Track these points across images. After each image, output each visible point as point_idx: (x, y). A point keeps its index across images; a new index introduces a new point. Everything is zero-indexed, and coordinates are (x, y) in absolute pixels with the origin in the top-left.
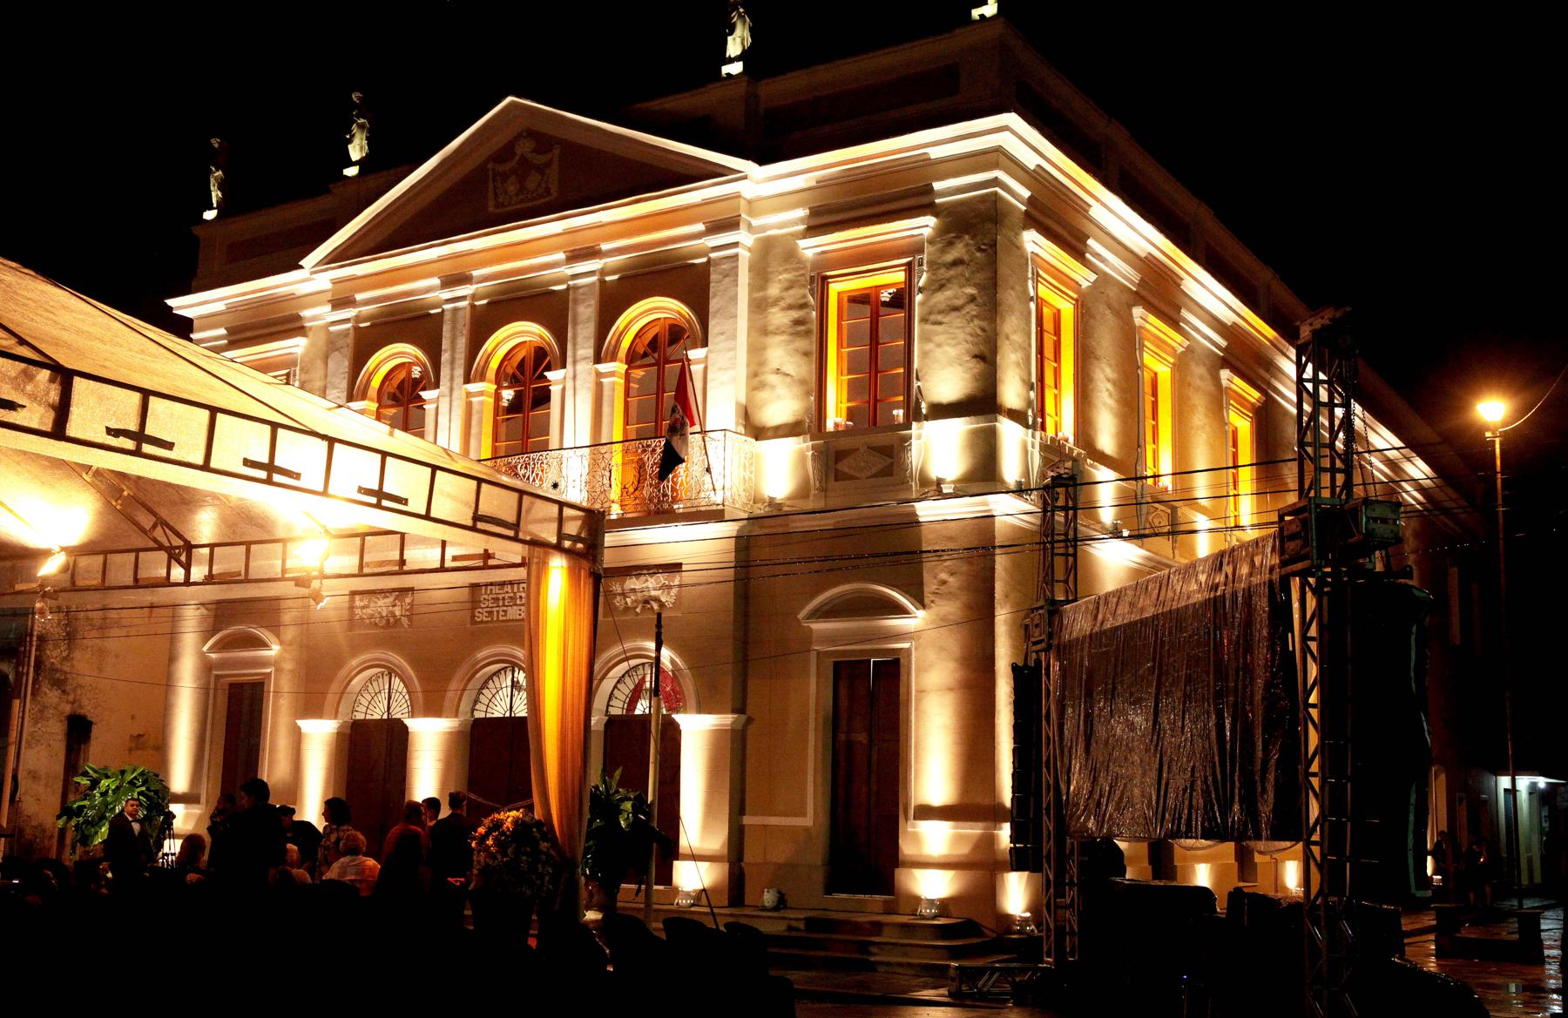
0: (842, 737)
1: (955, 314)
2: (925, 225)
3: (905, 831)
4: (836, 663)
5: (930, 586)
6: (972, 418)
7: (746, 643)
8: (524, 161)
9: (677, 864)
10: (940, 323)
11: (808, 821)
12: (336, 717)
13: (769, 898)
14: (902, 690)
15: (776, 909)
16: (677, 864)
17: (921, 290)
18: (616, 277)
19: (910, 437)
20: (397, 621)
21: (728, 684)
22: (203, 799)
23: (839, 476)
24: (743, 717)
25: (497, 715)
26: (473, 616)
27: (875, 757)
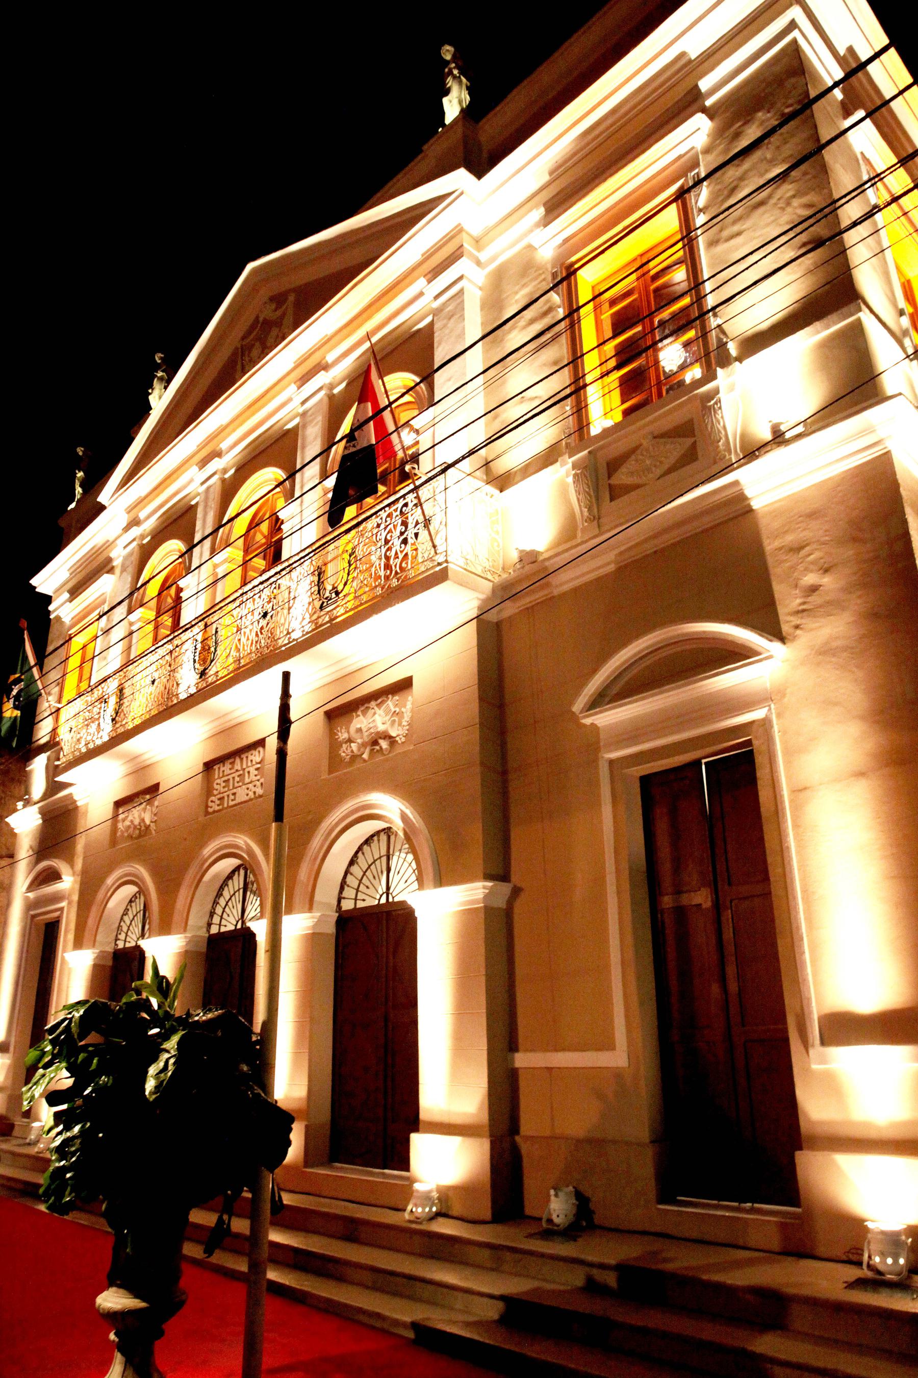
0: (667, 901)
1: (761, 210)
2: (695, 134)
3: (807, 1070)
4: (646, 781)
5: (787, 601)
6: (817, 325)
7: (504, 773)
8: (266, 322)
9: (415, 1138)
10: (739, 234)
11: (617, 1058)
12: (94, 946)
13: (559, 1208)
14: (764, 795)
15: (570, 1232)
16: (415, 1138)
17: (700, 210)
18: (344, 385)
19: (717, 391)
20: (147, 827)
21: (476, 833)
22: (12, 1049)
23: (615, 493)
24: (505, 889)
25: (231, 927)
26: (207, 806)
27: (728, 934)
